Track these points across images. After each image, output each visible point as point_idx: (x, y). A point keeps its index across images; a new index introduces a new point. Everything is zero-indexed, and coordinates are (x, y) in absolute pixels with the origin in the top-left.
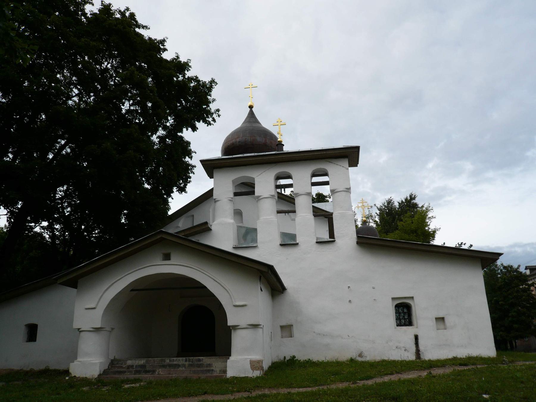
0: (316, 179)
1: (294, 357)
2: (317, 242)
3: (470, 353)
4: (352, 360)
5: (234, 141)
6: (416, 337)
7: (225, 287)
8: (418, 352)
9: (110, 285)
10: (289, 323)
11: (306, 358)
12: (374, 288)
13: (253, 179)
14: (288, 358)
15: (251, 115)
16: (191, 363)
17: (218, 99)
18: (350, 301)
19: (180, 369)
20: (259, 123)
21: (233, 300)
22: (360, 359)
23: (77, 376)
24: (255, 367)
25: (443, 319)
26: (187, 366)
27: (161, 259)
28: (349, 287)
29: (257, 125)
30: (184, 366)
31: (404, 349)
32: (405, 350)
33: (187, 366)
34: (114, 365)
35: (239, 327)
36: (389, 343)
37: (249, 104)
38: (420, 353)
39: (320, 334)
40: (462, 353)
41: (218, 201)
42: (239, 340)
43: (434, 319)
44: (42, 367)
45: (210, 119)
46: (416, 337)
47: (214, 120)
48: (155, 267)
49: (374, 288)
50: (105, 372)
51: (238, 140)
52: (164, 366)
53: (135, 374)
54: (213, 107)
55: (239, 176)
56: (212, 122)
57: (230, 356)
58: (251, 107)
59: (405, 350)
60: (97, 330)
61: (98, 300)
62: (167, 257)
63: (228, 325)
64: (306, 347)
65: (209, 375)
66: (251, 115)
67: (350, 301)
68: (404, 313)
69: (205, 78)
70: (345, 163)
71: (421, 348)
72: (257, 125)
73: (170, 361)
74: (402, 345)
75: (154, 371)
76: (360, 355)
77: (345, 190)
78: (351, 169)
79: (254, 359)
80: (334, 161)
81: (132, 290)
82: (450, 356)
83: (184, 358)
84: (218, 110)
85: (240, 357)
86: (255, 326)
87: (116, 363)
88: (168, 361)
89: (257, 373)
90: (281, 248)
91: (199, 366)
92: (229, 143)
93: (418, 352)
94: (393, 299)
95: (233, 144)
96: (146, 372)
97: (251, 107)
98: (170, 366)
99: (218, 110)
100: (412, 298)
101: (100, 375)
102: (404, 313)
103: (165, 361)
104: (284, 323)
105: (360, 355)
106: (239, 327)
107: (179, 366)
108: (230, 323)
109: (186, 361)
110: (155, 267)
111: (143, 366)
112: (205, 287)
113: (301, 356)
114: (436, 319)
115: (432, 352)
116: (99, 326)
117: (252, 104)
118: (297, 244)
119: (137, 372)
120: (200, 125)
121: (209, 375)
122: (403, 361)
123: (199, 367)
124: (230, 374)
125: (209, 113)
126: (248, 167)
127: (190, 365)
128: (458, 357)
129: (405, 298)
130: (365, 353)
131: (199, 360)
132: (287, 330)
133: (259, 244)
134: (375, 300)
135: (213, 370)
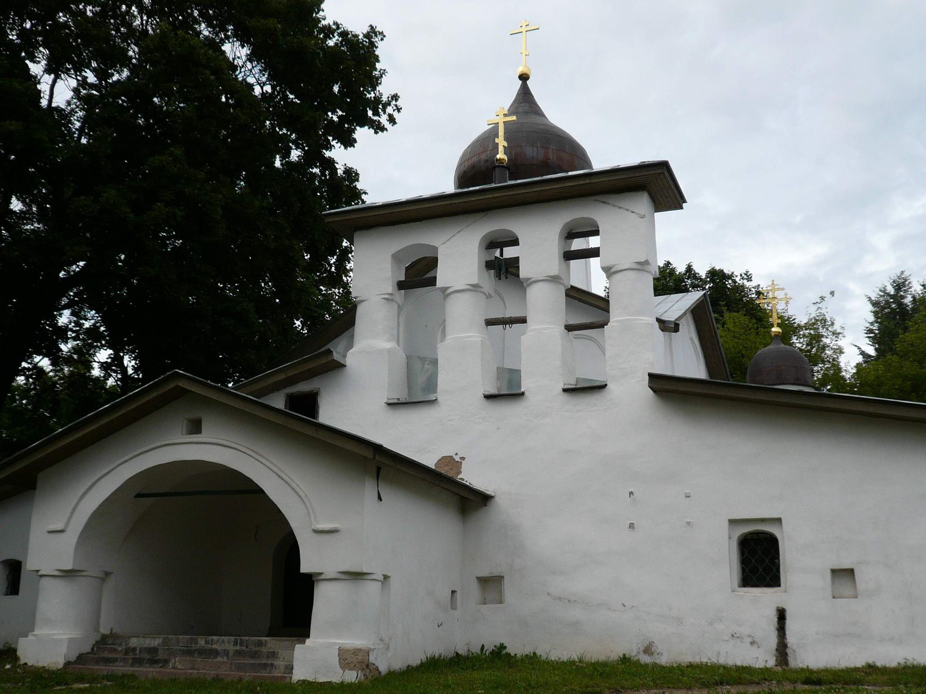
0: (578, 244)
1: (502, 647)
2: (565, 390)
3: (910, 658)
4: (625, 660)
5: (475, 159)
6: (782, 615)
7: (298, 490)
8: (782, 649)
9: (89, 484)
10: (496, 573)
11: (528, 650)
12: (688, 496)
13: (435, 249)
14: (489, 647)
15: (525, 98)
16: (238, 648)
17: (395, 73)
18: (632, 526)
19: (219, 659)
20: (543, 115)
21: (313, 520)
22: (645, 659)
23: (30, 664)
24: (348, 664)
25: (850, 572)
26: (231, 653)
27: (185, 430)
28: (631, 493)
29: (537, 120)
30: (226, 652)
31: (750, 640)
32: (752, 643)
33: (231, 653)
34: (104, 646)
35: (322, 577)
36: (729, 626)
37: (521, 70)
38: (789, 651)
39: (560, 599)
40: (891, 655)
41: (363, 301)
42: (326, 601)
43: (828, 575)
44: (451, 654)
45: (384, 119)
46: (782, 615)
47: (392, 120)
48: (218, 446)
49: (688, 496)
50: (81, 658)
51: (483, 157)
52: (189, 652)
53: (132, 665)
54: (385, 89)
55: (409, 244)
56: (387, 124)
57: (308, 636)
58: (524, 78)
59: (752, 643)
60: (68, 574)
61: (68, 515)
62: (195, 427)
63: (302, 571)
64: (520, 627)
65: (264, 674)
66: (525, 98)
67: (632, 526)
68: (759, 558)
69: (358, 28)
70: (642, 203)
71: (791, 639)
72: (537, 120)
73: (207, 642)
74: (745, 630)
75: (166, 662)
76: (648, 650)
77: (634, 266)
78: (660, 216)
79: (348, 647)
80: (613, 199)
81: (139, 496)
82: (859, 662)
83: (233, 638)
84: (395, 97)
85: (322, 641)
86: (356, 576)
87: (110, 642)
88: (202, 642)
89: (351, 676)
90: (565, 397)
91: (254, 655)
92: (467, 164)
93: (782, 649)
94: (733, 522)
95: (473, 167)
96: (153, 662)
97: (524, 78)
98: (202, 652)
99: (395, 97)
100: (779, 520)
101: (68, 664)
102: (759, 558)
103: (196, 643)
104: (485, 573)
105: (648, 650)
106: (322, 577)
107: (216, 653)
108: (305, 568)
109: (235, 644)
110: (218, 446)
111: (153, 650)
112: (262, 492)
113: (516, 648)
114: (834, 572)
115: (814, 652)
116: (69, 567)
117: (526, 71)
118: (523, 394)
119: (138, 661)
120: (362, 134)
121: (264, 674)
122: (720, 666)
123: (253, 657)
124: (299, 674)
125: (377, 104)
126: (372, 231)
127: (238, 653)
128: (879, 664)
129: (763, 520)
130: (659, 647)
131: (260, 644)
132: (491, 585)
133: (440, 395)
134: (688, 523)
135: (272, 665)
